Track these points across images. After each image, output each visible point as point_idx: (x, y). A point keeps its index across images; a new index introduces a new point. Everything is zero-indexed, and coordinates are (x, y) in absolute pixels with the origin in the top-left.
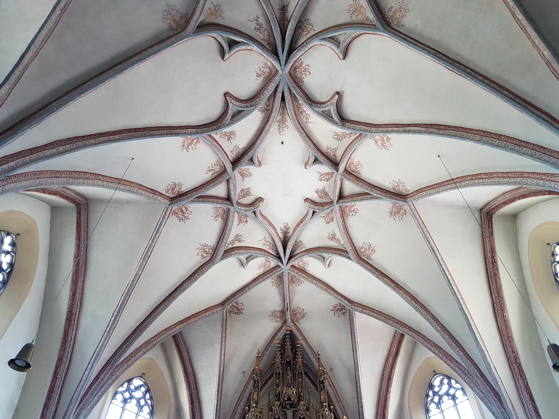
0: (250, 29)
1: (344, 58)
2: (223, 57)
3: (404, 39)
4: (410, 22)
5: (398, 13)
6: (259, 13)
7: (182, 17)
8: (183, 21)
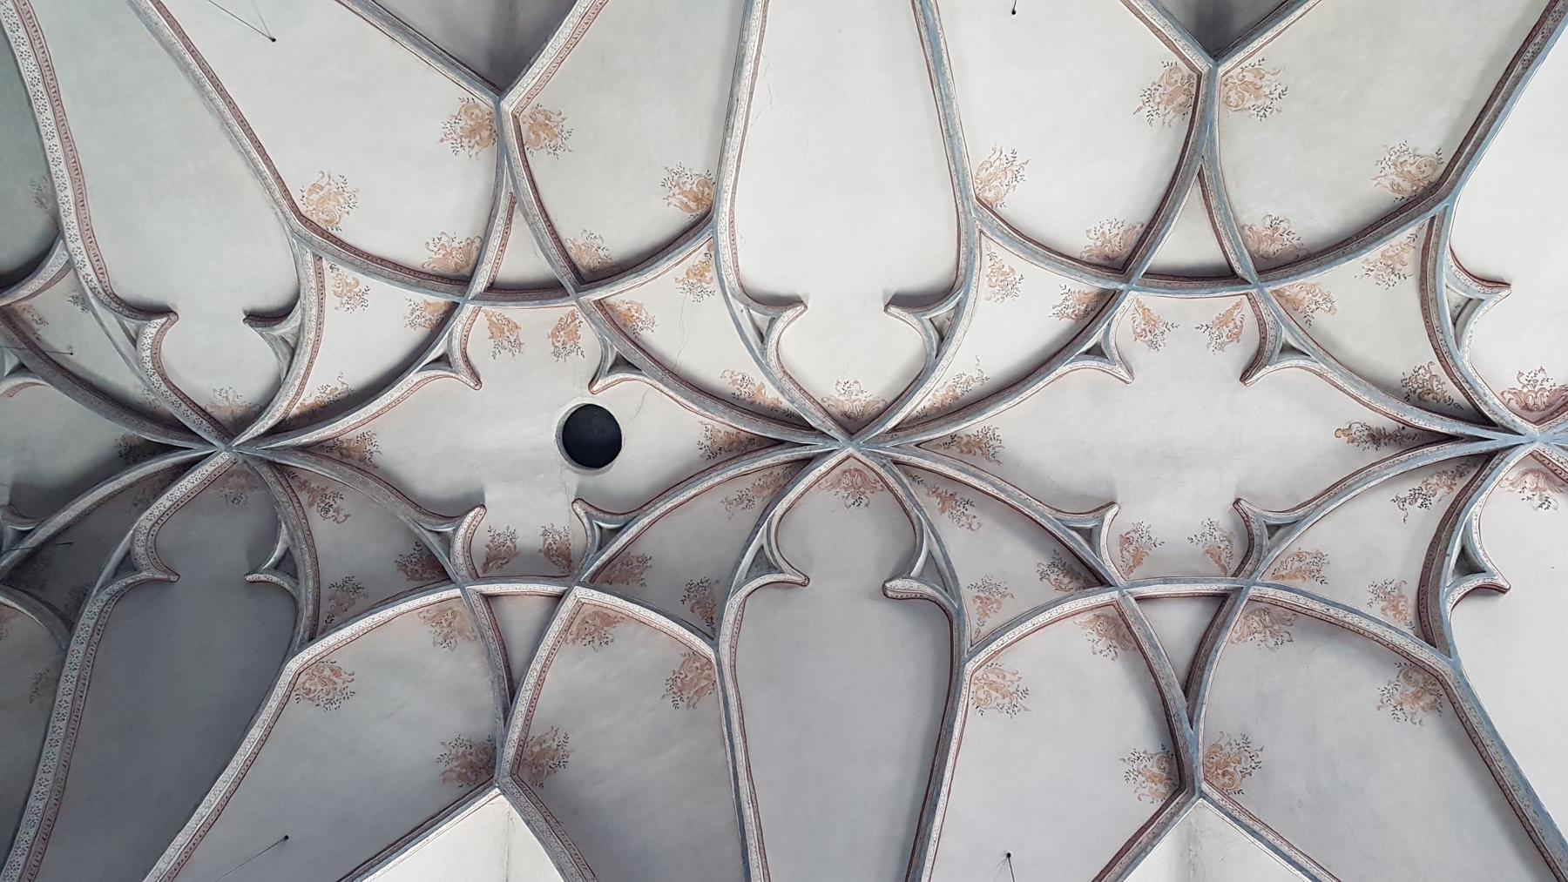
0: (1425, 520)
1: (1507, 285)
2: (1502, 590)
3: (1477, 146)
4: (1430, 139)
5: (1407, 168)
6: (1387, 495)
7: (1407, 677)
8: (1415, 676)
